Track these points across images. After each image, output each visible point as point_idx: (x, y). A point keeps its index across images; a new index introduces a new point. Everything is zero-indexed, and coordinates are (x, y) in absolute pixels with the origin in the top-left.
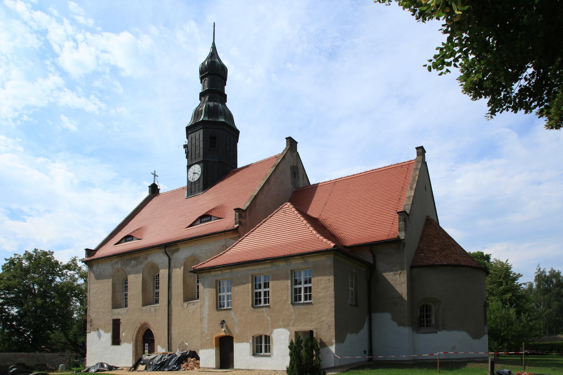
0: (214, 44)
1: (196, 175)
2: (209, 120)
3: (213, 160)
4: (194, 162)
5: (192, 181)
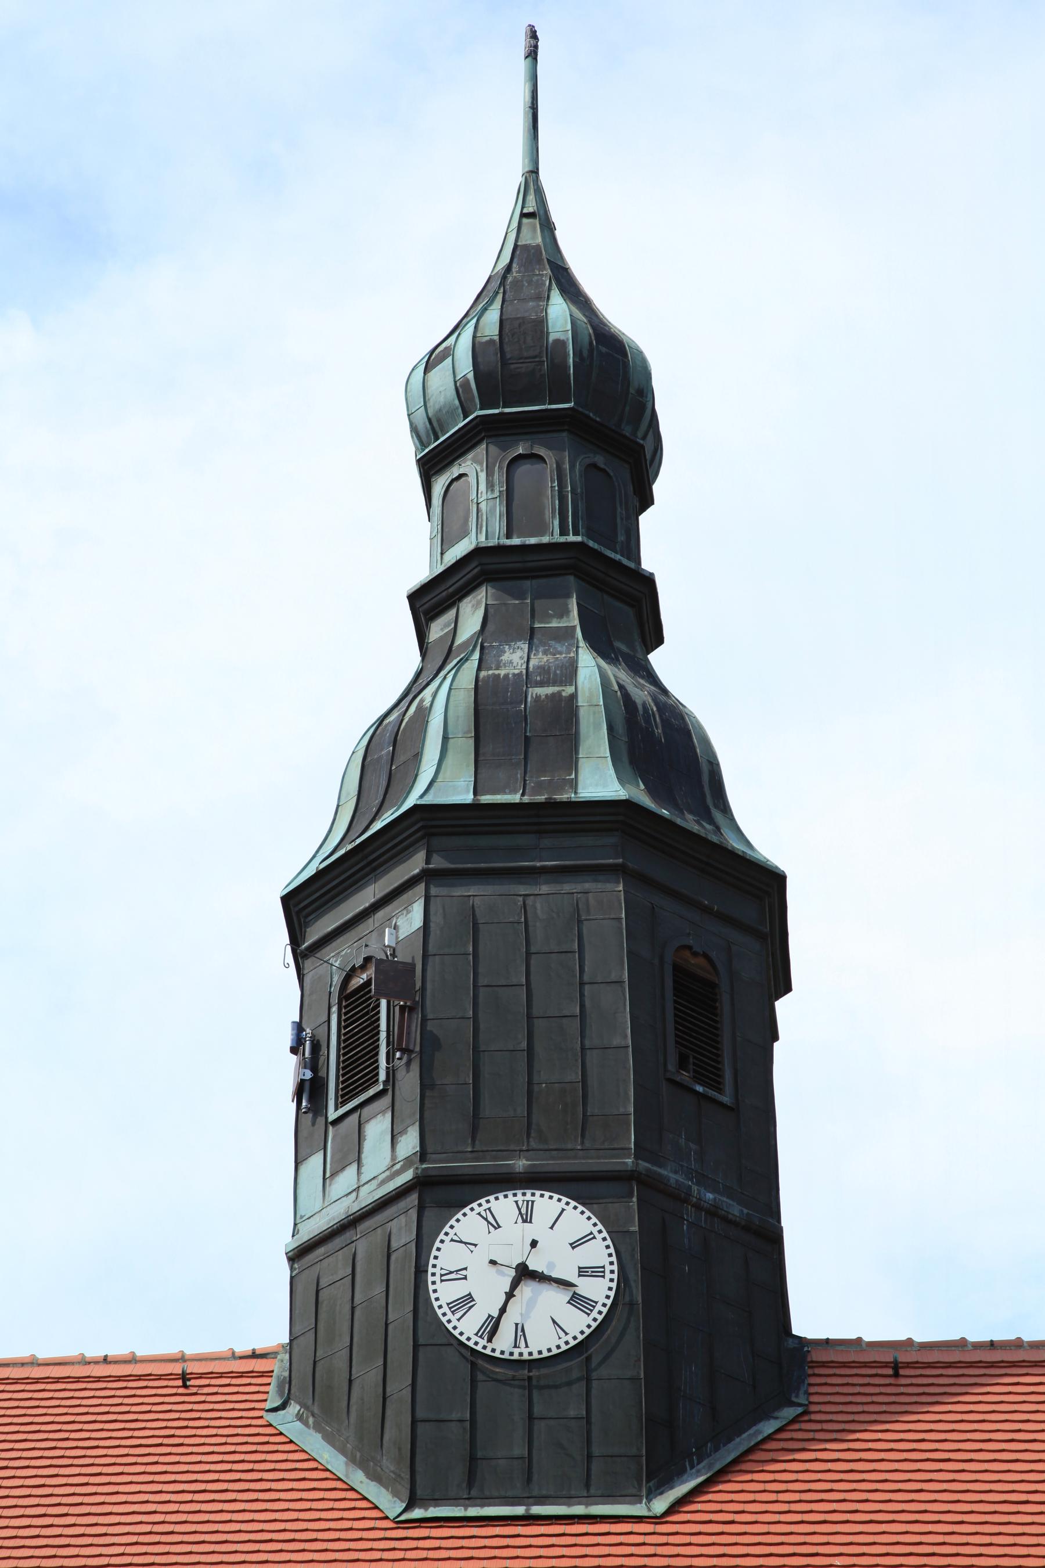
0: (533, 174)
1: (554, 1300)
2: (486, 799)
3: (710, 1196)
4: (521, 1164)
5: (480, 1345)
